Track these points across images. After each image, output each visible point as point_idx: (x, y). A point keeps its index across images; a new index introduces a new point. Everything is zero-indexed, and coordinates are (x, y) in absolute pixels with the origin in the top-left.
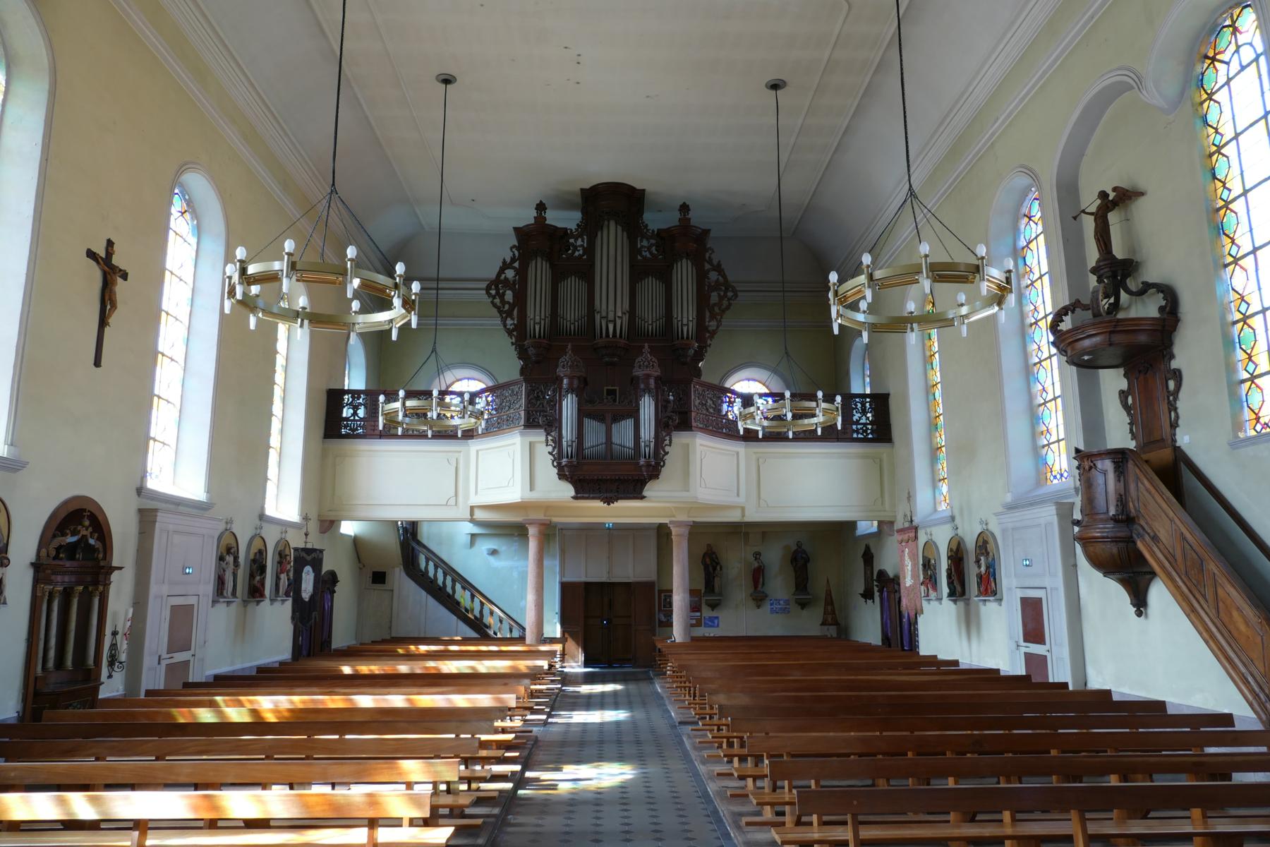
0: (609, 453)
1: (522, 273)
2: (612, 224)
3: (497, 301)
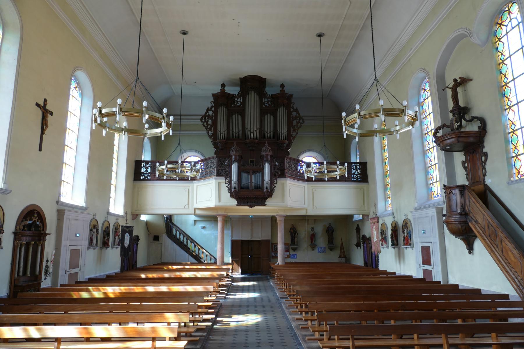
0: (251, 187)
1: (215, 113)
2: (253, 92)
3: (205, 124)
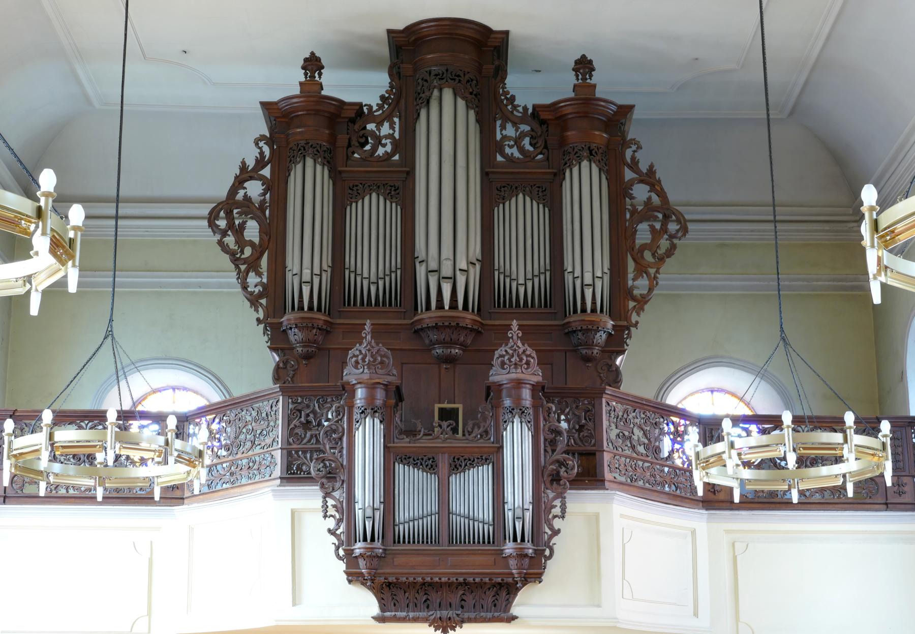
0: (445, 535)
1: (277, 188)
2: (448, 95)
3: (230, 240)
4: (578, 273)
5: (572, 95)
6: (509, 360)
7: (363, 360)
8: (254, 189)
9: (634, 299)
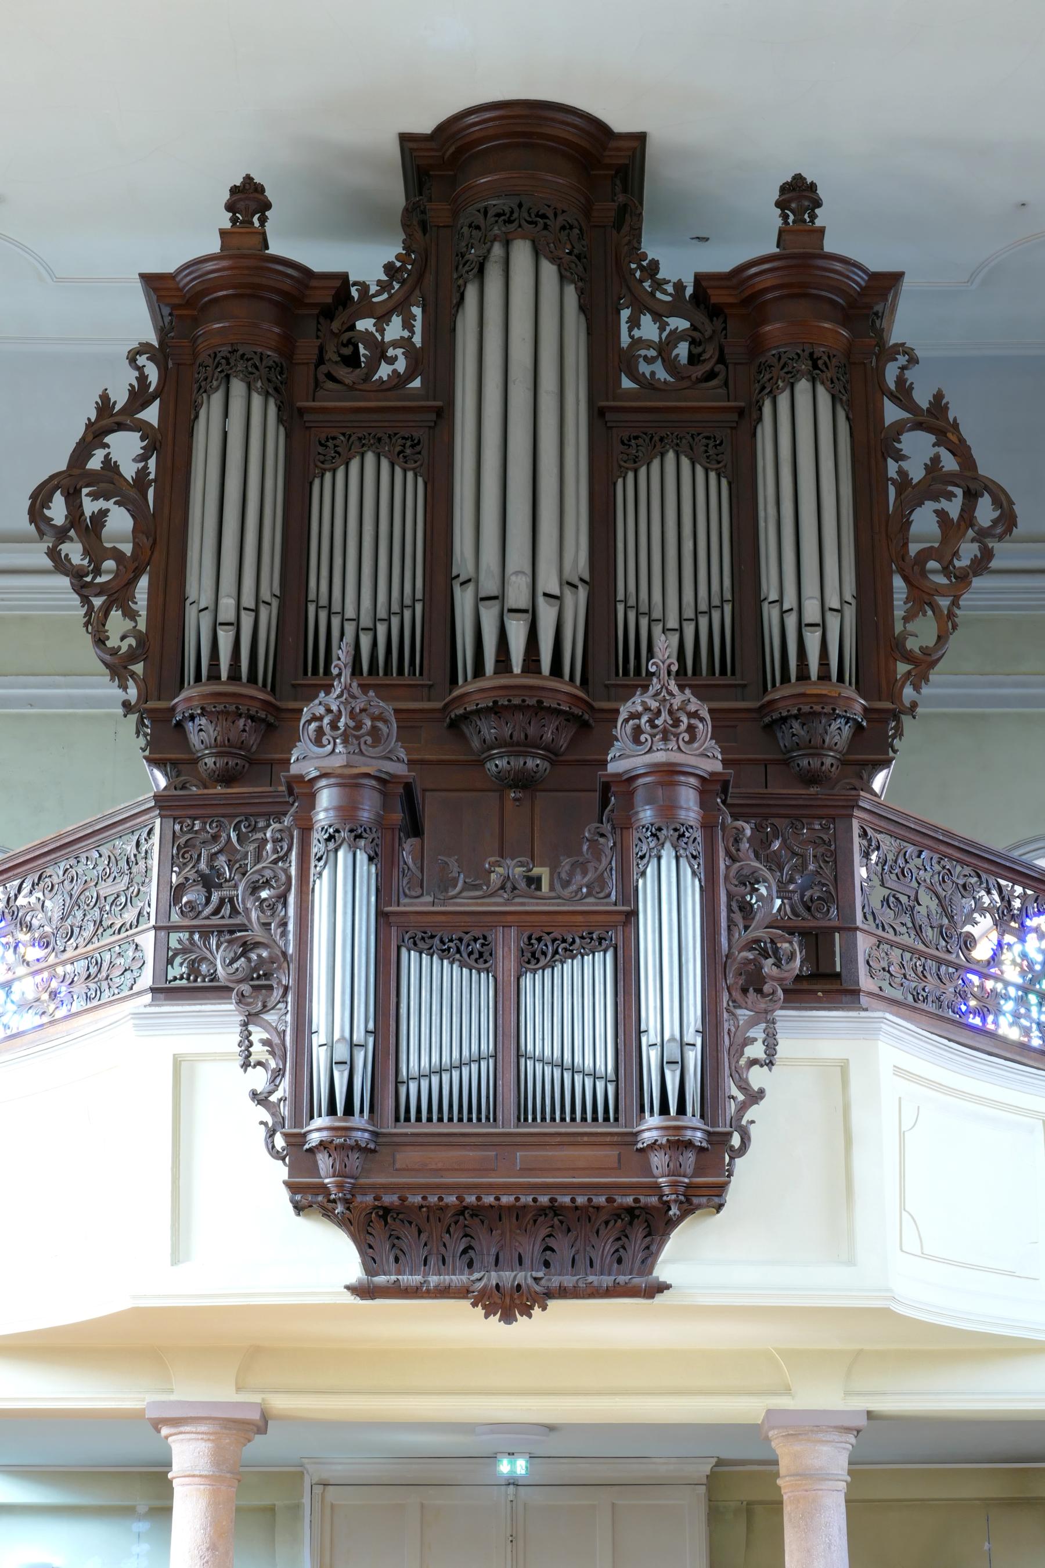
0: (509, 1104)
1: (171, 446)
2: (522, 254)
3: (74, 551)
4: (790, 602)
5: (773, 249)
6: (651, 722)
7: (334, 726)
8: (125, 449)
9: (908, 657)
